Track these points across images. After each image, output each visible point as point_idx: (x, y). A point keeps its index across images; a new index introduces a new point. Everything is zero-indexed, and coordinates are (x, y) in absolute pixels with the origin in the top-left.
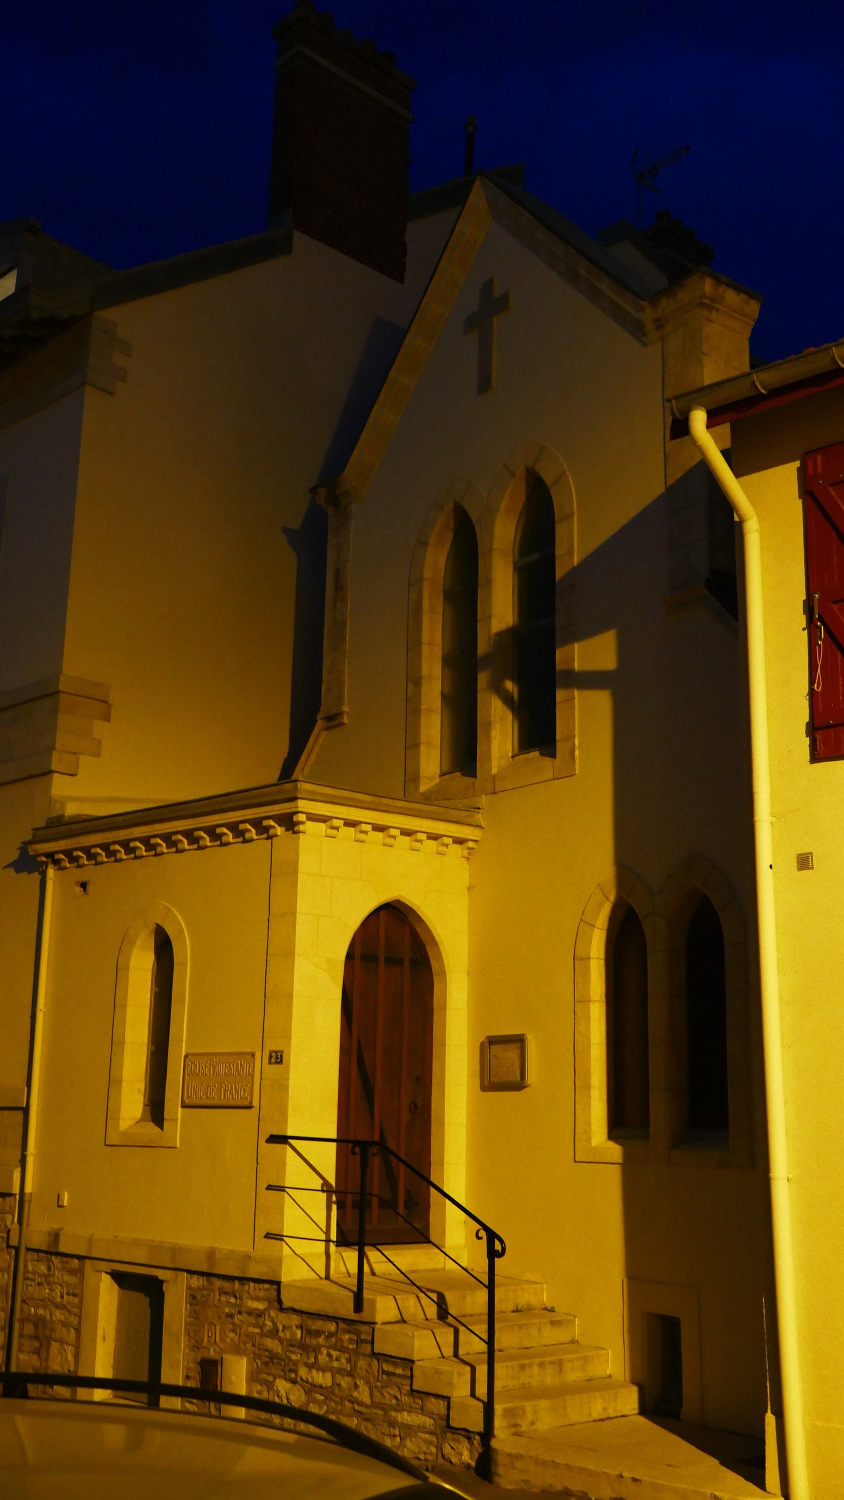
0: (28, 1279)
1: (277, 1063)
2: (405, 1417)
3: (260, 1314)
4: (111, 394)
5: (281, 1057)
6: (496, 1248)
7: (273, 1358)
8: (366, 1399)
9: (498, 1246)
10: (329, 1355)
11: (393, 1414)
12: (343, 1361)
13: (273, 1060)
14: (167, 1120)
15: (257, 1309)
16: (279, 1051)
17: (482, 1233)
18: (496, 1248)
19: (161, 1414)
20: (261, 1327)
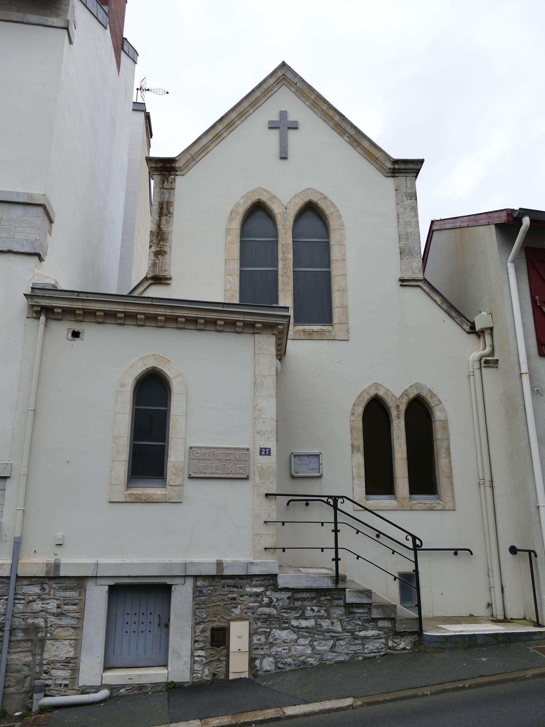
0: (17, 599)
1: (265, 455)
2: (362, 634)
3: (257, 595)
4: (297, 128)
5: (269, 451)
6: (417, 543)
7: (267, 619)
8: (340, 629)
9: (418, 542)
10: (312, 610)
11: (357, 633)
12: (322, 611)
13: (263, 453)
14: (123, 461)
15: (256, 592)
16: (267, 448)
17: (410, 538)
18: (417, 543)
19: (12, 575)
20: (261, 602)
